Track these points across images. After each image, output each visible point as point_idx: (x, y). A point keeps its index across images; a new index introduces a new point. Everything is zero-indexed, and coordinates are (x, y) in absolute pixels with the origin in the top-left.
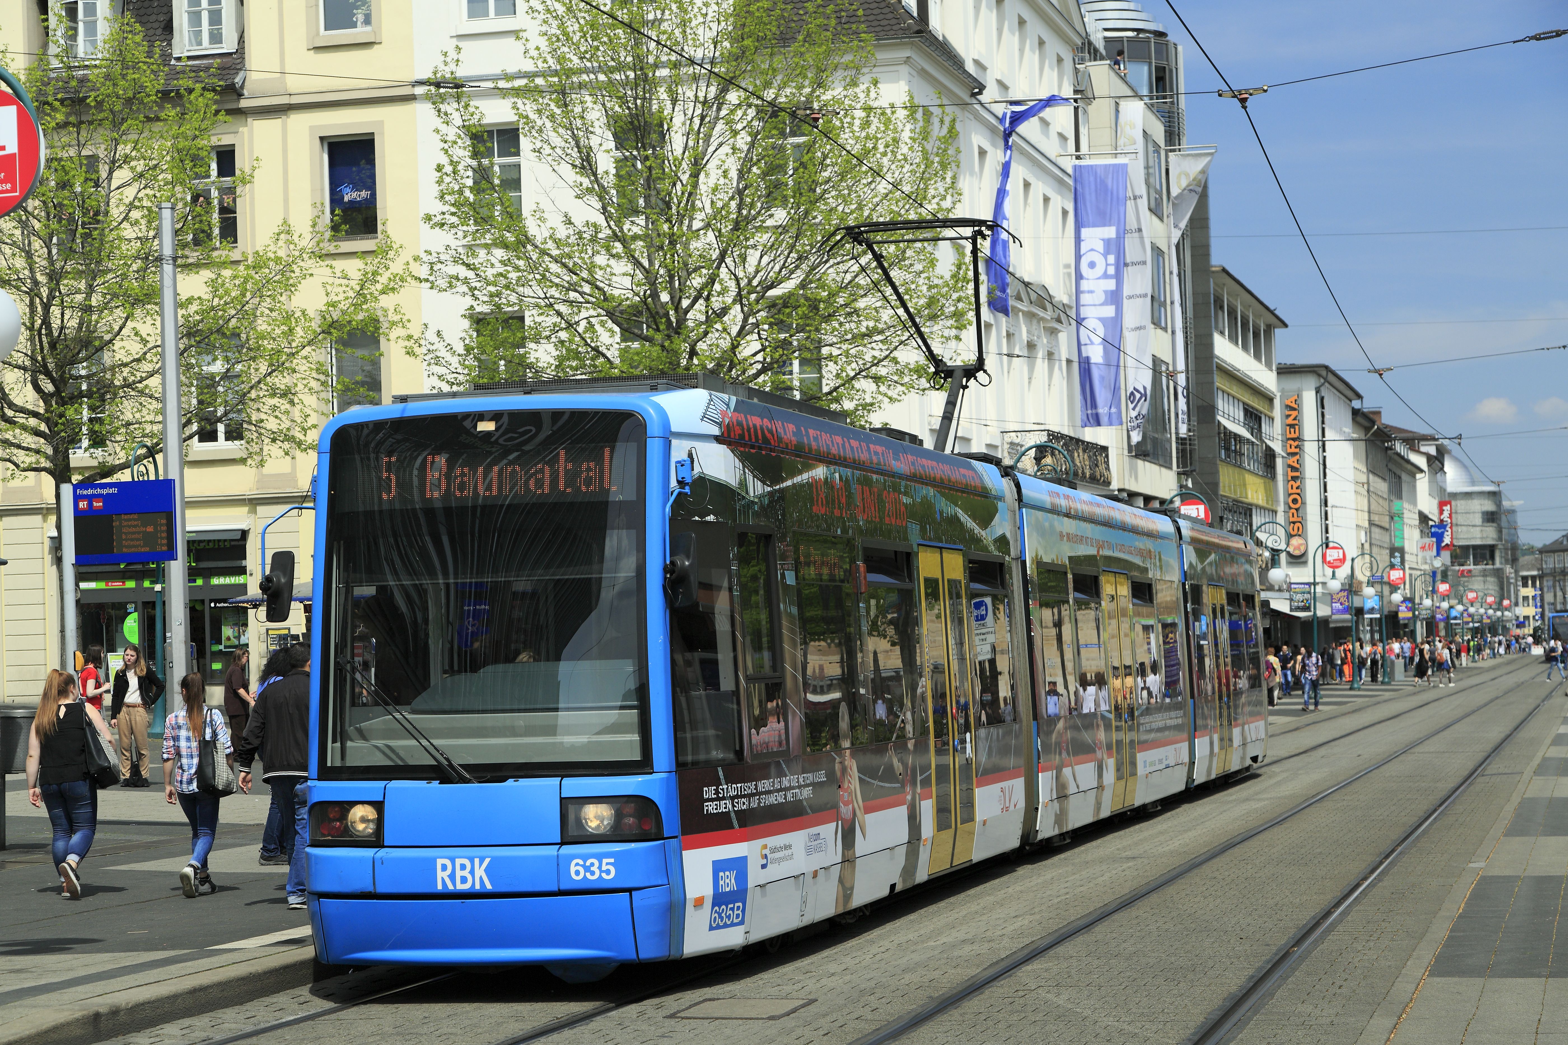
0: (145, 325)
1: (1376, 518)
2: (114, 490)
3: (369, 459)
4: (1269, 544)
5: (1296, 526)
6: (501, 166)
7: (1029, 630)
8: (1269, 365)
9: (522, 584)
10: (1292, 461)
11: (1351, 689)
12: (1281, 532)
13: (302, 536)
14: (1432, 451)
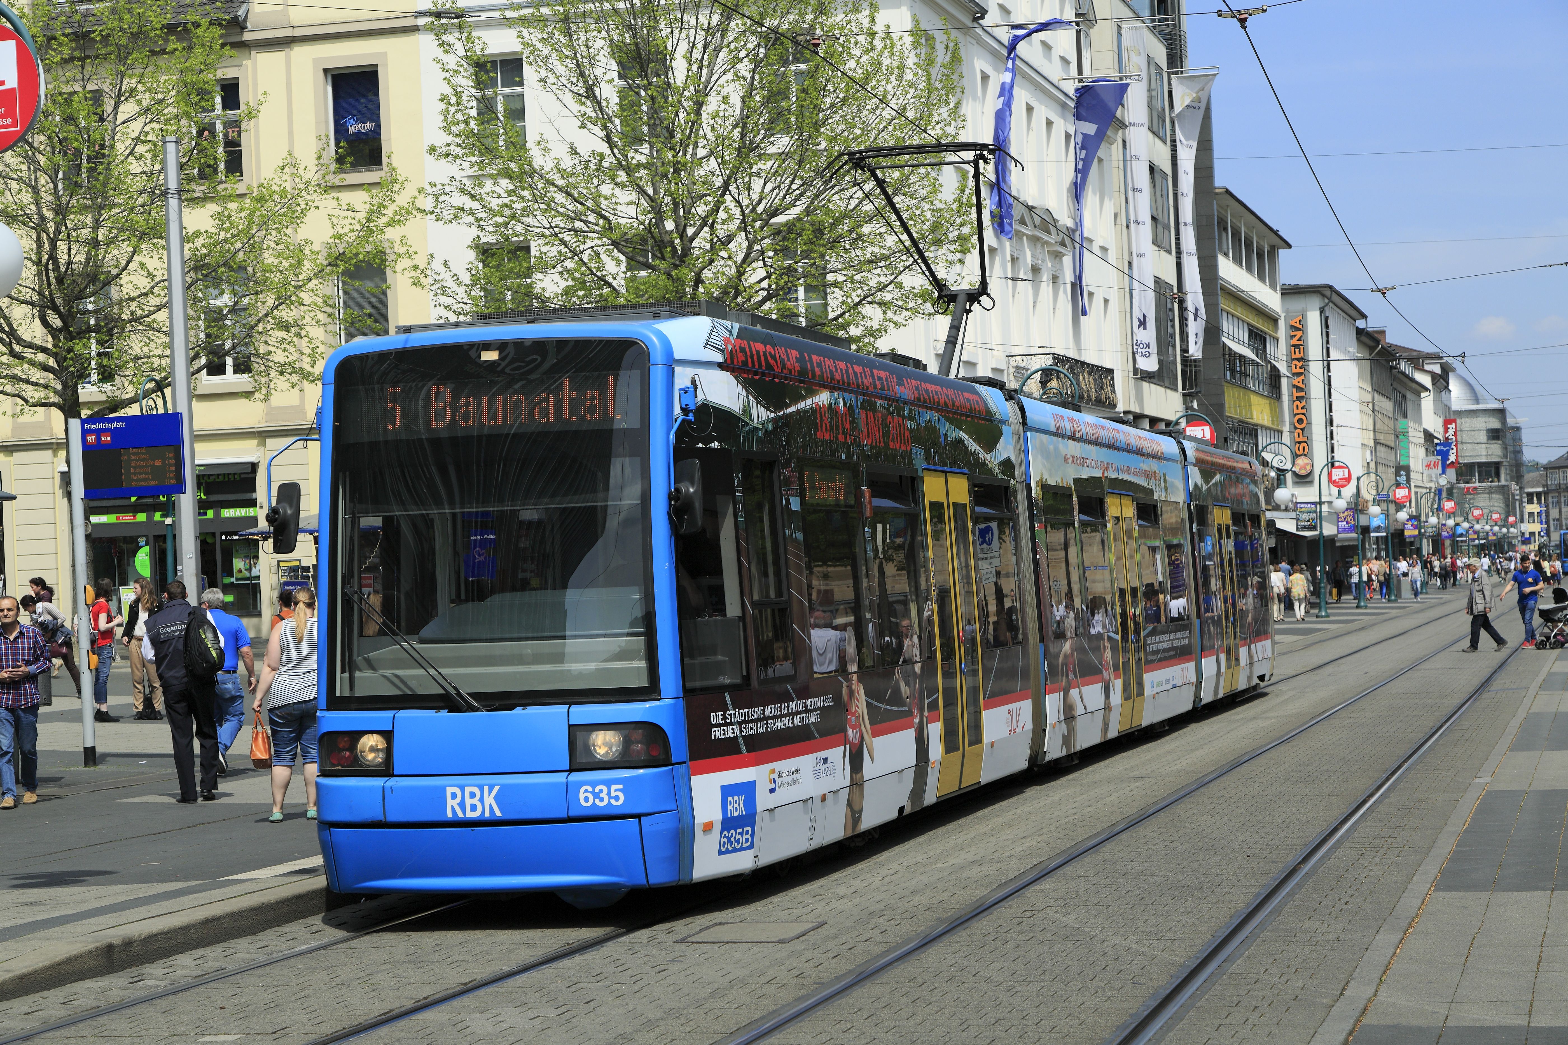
1: (1381, 437)
2: (121, 425)
3: (373, 389)
4: (1275, 464)
5: (1302, 446)
7: (1035, 553)
9: (529, 514)
10: (1297, 381)
11: (1358, 607)
12: (1287, 452)
13: (305, 467)
14: (1437, 369)
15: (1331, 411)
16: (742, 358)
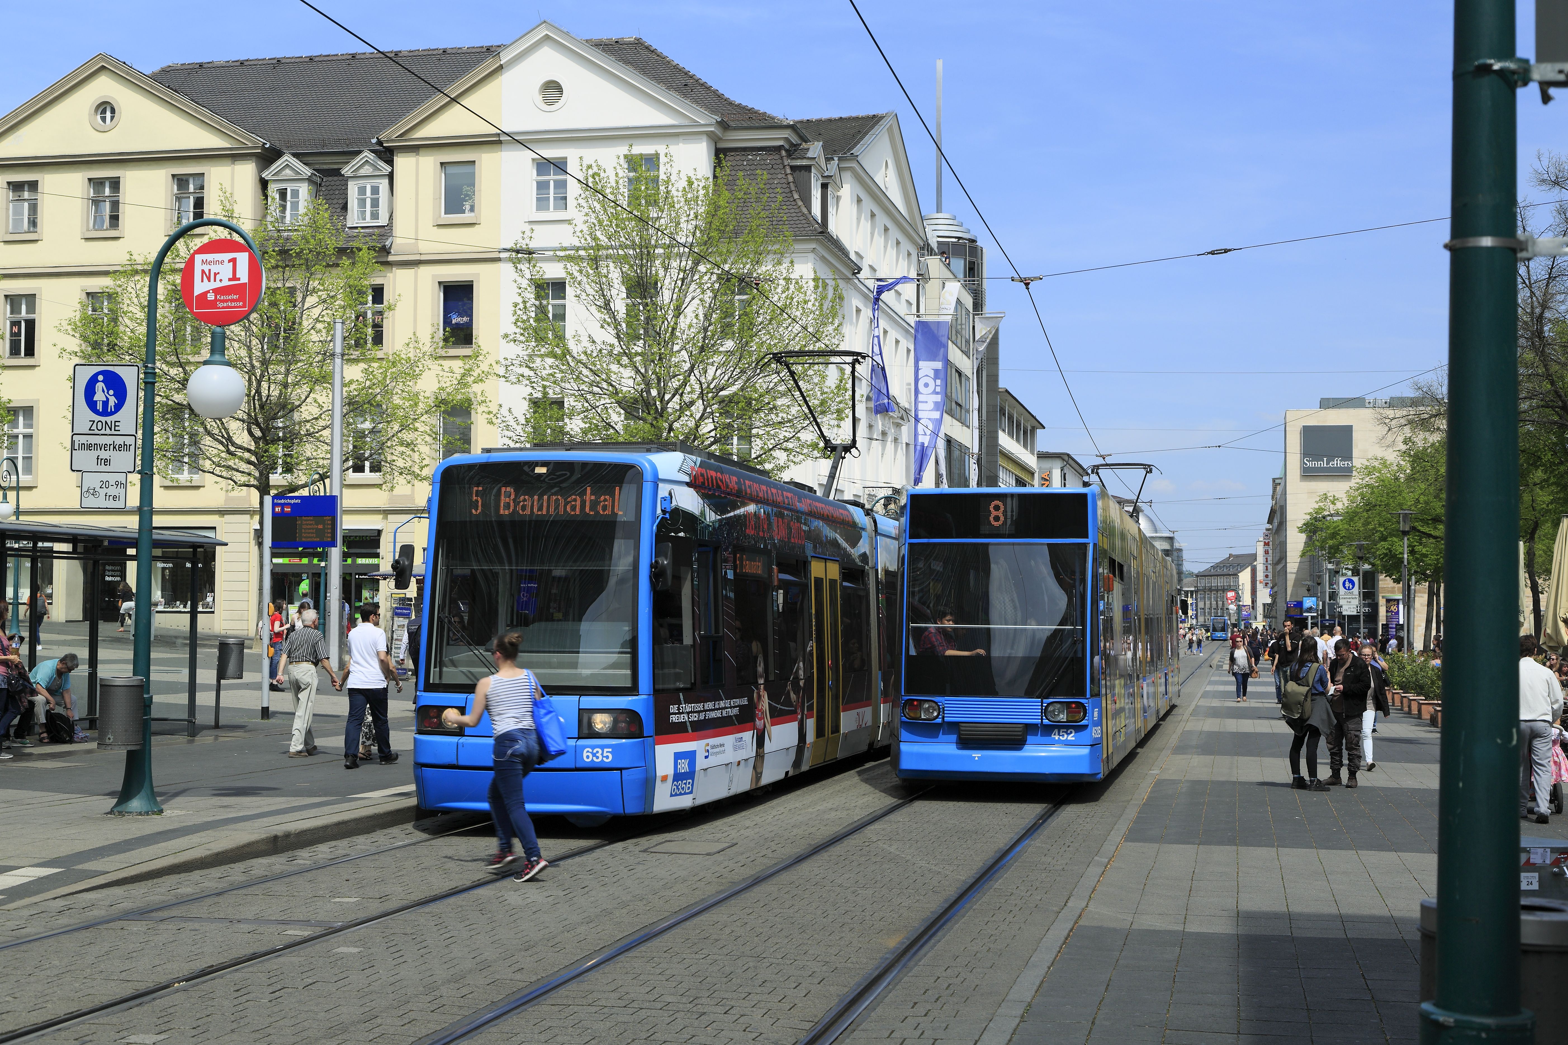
0: (322, 396)
2: (299, 501)
6: (554, 306)
8: (1032, 453)
13: (420, 534)
16: (701, 480)
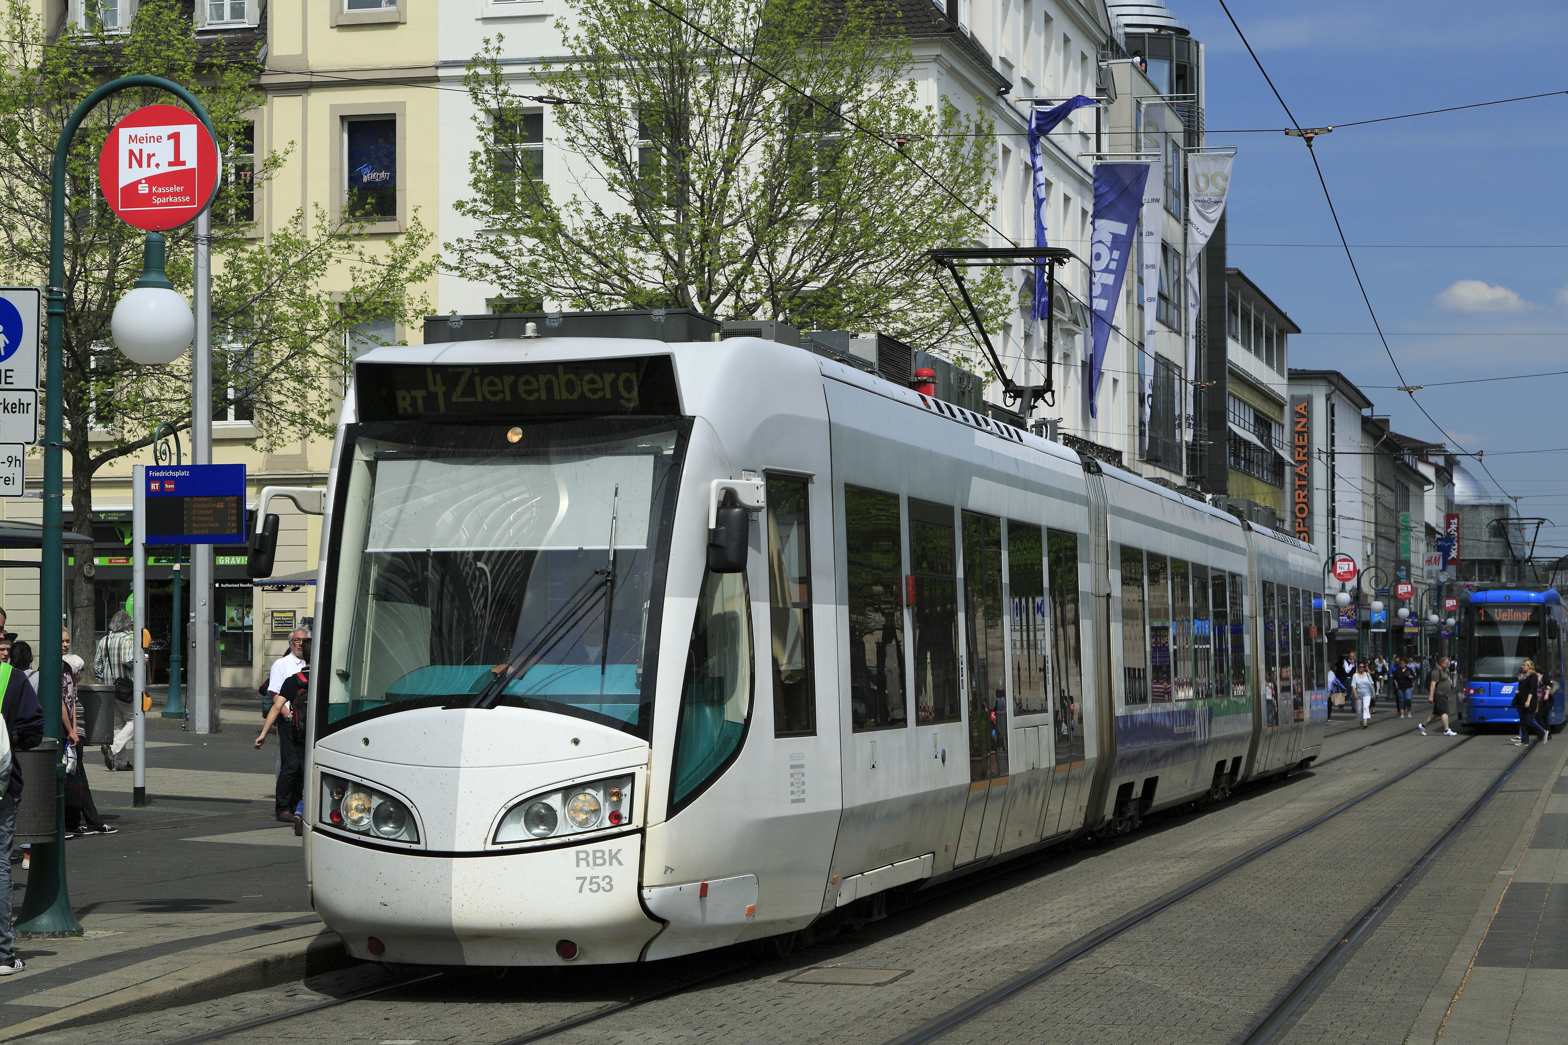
8: (1280, 372)
15: (1333, 501)
